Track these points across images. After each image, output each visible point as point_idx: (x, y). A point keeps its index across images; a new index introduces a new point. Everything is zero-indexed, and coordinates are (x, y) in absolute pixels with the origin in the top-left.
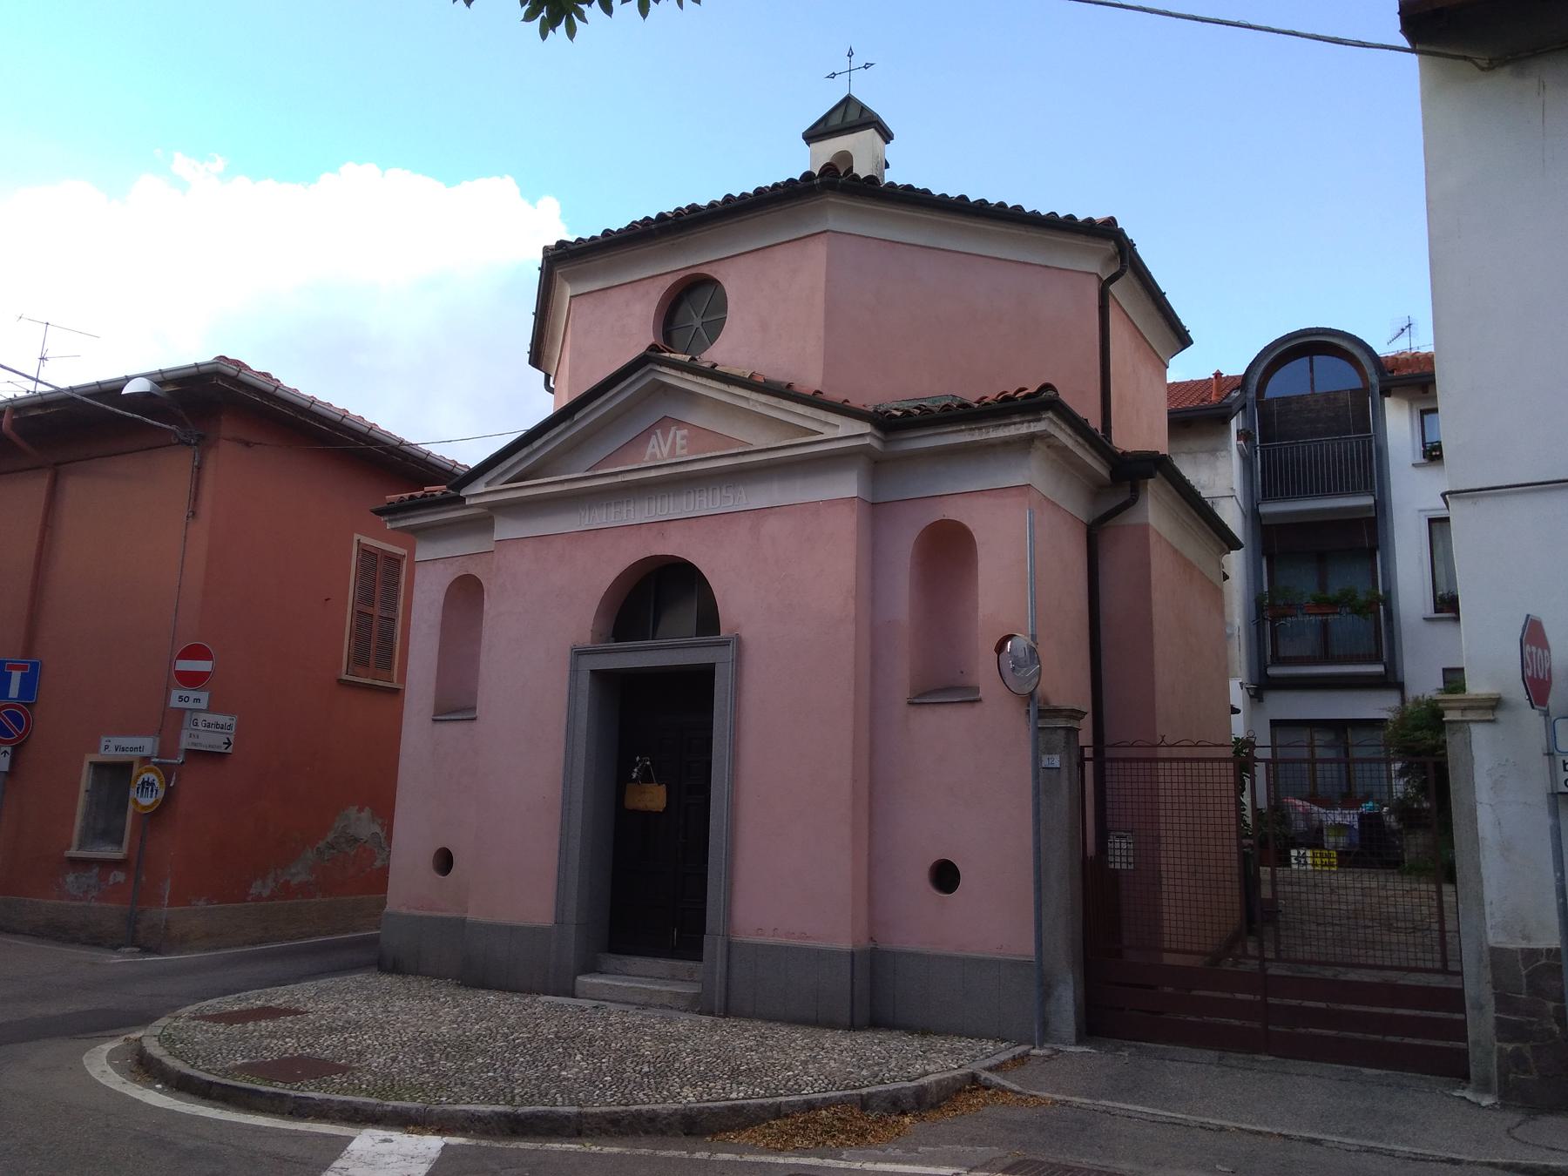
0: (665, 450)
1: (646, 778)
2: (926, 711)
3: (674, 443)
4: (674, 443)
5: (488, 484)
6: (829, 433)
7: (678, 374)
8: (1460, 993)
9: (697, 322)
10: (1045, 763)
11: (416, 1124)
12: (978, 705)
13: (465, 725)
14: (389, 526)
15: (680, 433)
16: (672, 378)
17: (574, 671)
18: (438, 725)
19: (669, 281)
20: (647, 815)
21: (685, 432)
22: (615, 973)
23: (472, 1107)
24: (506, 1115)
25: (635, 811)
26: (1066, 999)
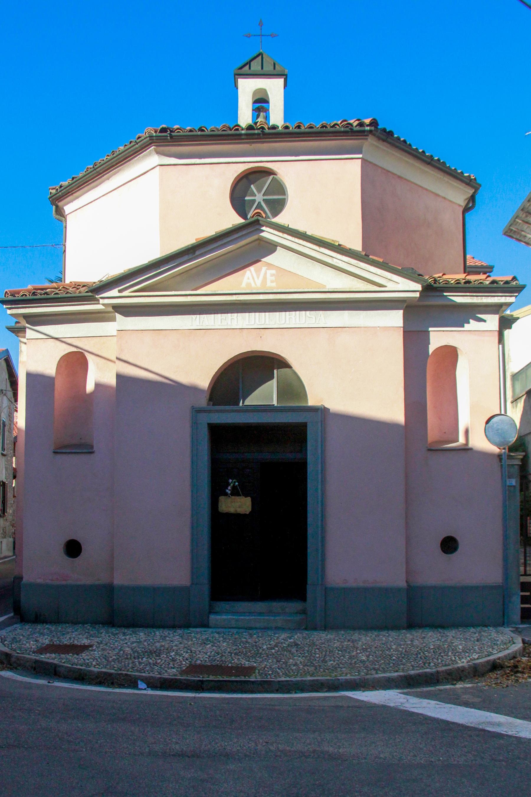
0: (251, 281)
1: (235, 493)
2: (64, 457)
3: (265, 278)
4: (265, 278)
5: (120, 291)
6: (391, 286)
7: (280, 234)
8: (522, 603)
9: (259, 198)
10: (508, 483)
11: (364, 687)
12: (92, 455)
13: (84, 457)
14: (9, 312)
15: (269, 272)
16: (268, 234)
17: (195, 424)
18: (59, 456)
19: (242, 168)
20: (237, 516)
21: (274, 272)
22: (227, 612)
23: (387, 675)
24: (405, 676)
25: (228, 515)
26: (516, 606)
